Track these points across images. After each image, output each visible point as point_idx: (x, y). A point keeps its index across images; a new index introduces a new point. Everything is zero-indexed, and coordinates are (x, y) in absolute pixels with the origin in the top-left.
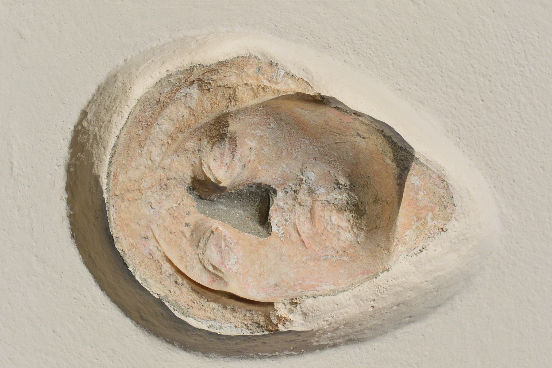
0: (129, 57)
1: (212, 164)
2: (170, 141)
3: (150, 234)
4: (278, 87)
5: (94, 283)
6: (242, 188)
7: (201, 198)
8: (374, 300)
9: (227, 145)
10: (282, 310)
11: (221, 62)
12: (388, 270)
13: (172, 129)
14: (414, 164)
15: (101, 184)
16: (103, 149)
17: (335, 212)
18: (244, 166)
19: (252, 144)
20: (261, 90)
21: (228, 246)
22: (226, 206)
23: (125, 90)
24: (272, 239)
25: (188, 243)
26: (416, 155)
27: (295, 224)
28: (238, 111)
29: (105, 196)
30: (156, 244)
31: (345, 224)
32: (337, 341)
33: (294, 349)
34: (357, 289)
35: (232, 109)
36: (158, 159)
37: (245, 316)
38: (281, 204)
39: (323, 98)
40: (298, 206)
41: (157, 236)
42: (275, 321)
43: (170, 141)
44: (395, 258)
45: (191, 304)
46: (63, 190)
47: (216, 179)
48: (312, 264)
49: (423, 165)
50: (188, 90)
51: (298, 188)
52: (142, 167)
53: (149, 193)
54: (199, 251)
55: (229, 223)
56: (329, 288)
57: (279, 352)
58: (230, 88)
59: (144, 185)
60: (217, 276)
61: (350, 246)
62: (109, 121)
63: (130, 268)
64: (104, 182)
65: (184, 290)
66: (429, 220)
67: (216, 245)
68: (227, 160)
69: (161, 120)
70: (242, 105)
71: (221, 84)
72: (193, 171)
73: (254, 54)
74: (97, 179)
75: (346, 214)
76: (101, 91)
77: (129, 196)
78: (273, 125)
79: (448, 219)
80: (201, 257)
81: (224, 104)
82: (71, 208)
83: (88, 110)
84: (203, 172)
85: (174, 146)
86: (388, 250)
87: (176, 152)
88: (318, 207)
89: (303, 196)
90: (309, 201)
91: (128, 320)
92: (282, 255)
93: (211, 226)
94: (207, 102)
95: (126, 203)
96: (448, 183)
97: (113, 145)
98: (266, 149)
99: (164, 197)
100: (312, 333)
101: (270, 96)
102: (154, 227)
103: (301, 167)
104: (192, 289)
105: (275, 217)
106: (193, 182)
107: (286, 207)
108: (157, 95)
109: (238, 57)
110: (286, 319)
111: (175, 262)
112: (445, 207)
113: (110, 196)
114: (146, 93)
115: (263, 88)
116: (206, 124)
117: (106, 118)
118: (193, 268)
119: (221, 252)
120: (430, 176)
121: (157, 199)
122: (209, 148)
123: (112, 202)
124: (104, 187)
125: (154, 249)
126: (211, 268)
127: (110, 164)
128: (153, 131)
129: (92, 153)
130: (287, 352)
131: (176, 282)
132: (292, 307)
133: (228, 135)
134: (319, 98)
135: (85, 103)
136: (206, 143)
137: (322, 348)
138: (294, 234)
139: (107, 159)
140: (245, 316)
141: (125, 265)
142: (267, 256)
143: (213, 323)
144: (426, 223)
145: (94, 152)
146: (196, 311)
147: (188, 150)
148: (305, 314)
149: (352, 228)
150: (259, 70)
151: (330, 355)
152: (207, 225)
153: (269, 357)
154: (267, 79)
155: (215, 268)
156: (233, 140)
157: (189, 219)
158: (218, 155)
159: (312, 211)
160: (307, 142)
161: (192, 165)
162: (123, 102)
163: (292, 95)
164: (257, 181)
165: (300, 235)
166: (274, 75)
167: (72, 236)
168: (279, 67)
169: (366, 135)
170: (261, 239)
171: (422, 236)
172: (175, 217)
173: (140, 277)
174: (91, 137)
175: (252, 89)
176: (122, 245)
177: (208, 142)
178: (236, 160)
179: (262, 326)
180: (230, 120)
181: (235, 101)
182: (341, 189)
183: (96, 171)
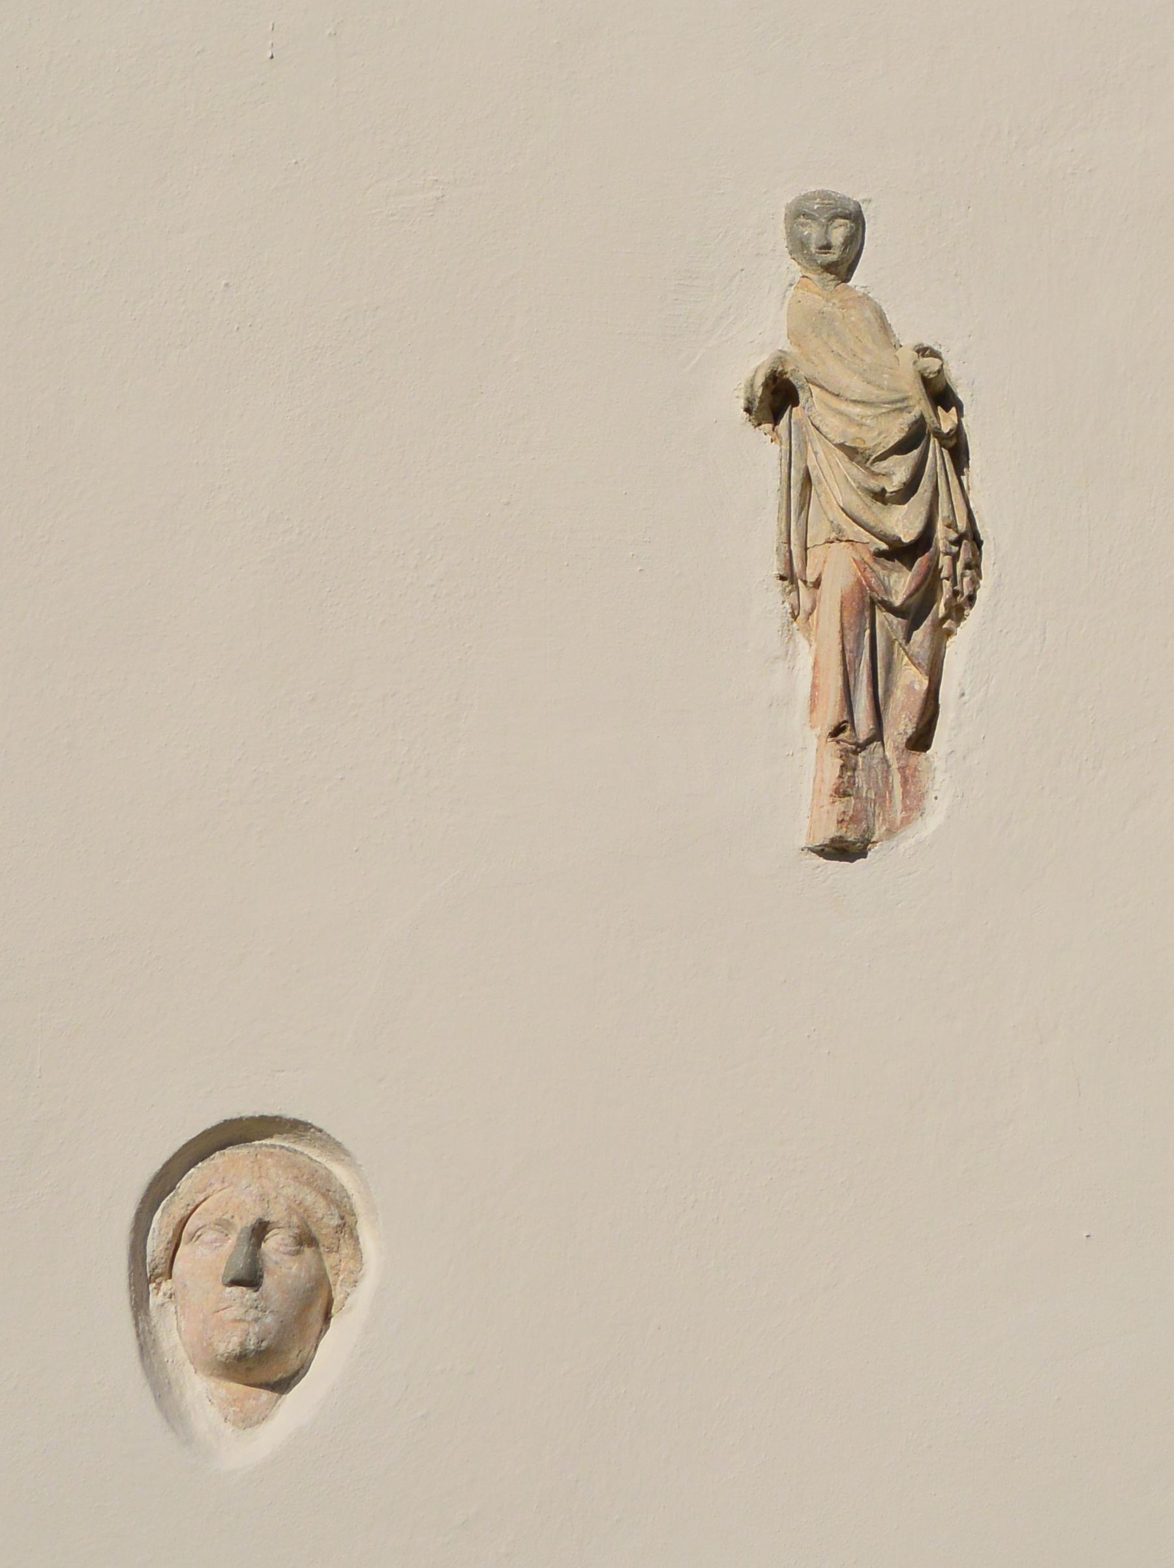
0: (363, 1169)
1: (279, 1237)
3: (226, 1184)
4: (338, 1286)
5: (189, 1139)
6: (260, 1262)
7: (253, 1230)
8: (173, 1361)
9: (293, 1248)
10: (166, 1286)
11: (358, 1239)
12: (196, 1372)
13: (307, 1204)
14: (277, 1395)
15: (266, 1140)
16: (293, 1141)
17: (240, 1340)
18: (277, 1263)
19: (294, 1270)
20: (336, 1272)
23: (339, 1161)
24: (220, 1287)
25: (218, 1217)
26: (283, 1396)
27: (231, 1307)
28: (320, 1254)
29: (257, 1142)
30: (219, 1189)
31: (231, 1347)
32: (142, 1337)
33: (136, 1302)
34: (182, 1348)
35: (322, 1249)
36: (284, 1192)
37: (162, 1258)
38: (247, 1296)
39: (330, 1319)
40: (246, 1309)
41: (224, 1191)
42: (158, 1281)
43: (297, 1202)
44: (205, 1379)
46: (261, 1114)
47: (267, 1239)
49: (276, 1401)
50: (337, 1216)
51: (259, 1309)
52: (278, 1180)
53: (257, 1185)
54: (212, 1225)
56: (183, 1325)
57: (134, 1290)
58: (338, 1248)
59: (264, 1181)
60: (193, 1237)
62: (315, 1147)
63: (200, 1164)
64: (267, 1142)
65: (182, 1212)
66: (233, 1409)
67: (216, 1239)
68: (282, 1249)
69: (314, 1193)
70: (324, 1257)
71: (341, 1242)
72: (273, 1222)
73: (364, 1268)
74: (270, 1136)
75: (239, 1348)
76: (338, 1145)
77: (256, 1168)
78: (308, 1285)
80: (208, 1227)
81: (326, 1244)
82: (247, 1119)
83: (323, 1133)
84: (273, 1229)
85: (294, 1206)
86: (211, 1375)
87: (289, 1208)
88: (243, 1326)
89: (253, 1313)
90: (249, 1318)
91: (160, 1167)
92: (208, 1293)
95: (250, 1165)
96: (261, 1423)
98: (290, 1282)
99: (254, 1198)
100: (147, 1314)
101: (331, 1279)
102: (231, 1188)
104: (184, 1217)
105: (237, 1291)
106: (265, 1222)
107: (245, 1300)
108: (333, 1189)
109: (362, 1254)
110: (159, 1289)
112: (243, 1421)
113: (256, 1148)
114: (336, 1178)
115: (337, 1273)
116: (310, 1231)
117: (317, 1144)
118: (200, 1219)
119: (212, 1243)
120: (267, 1409)
121: (254, 1192)
122: (291, 1234)
123: (252, 1150)
124: (264, 1142)
125: (214, 1188)
126: (199, 1233)
127: (282, 1147)
128: (306, 1187)
129: (290, 1133)
130: (133, 1296)
131: (188, 1205)
133: (302, 1248)
134: (329, 1316)
135: (328, 1132)
137: (137, 1325)
138: (225, 1305)
139: (286, 1144)
140: (162, 1258)
141: (202, 1160)
143: (157, 1233)
144: (231, 1407)
145: (291, 1135)
146: (166, 1220)
147: (290, 1217)
148: (163, 1305)
150: (352, 1272)
151: (132, 1332)
152: (232, 1232)
153: (130, 1282)
154: (344, 1278)
155: (199, 1236)
156: (298, 1252)
157: (237, 1218)
158: (286, 1242)
160: (295, 1314)
161: (278, 1221)
162: (329, 1158)
163: (331, 1295)
164: (265, 1275)
165: (223, 1310)
166: (347, 1284)
167: (226, 1121)
168: (354, 1288)
169: (299, 1357)
170: (221, 1277)
172: (238, 1207)
173: (193, 1173)
174: (303, 1133)
175: (337, 1265)
176: (218, 1158)
177: (296, 1233)
178: (281, 1255)
179: (154, 1271)
180: (313, 1248)
181: (328, 1252)
182: (258, 1343)
183: (276, 1136)
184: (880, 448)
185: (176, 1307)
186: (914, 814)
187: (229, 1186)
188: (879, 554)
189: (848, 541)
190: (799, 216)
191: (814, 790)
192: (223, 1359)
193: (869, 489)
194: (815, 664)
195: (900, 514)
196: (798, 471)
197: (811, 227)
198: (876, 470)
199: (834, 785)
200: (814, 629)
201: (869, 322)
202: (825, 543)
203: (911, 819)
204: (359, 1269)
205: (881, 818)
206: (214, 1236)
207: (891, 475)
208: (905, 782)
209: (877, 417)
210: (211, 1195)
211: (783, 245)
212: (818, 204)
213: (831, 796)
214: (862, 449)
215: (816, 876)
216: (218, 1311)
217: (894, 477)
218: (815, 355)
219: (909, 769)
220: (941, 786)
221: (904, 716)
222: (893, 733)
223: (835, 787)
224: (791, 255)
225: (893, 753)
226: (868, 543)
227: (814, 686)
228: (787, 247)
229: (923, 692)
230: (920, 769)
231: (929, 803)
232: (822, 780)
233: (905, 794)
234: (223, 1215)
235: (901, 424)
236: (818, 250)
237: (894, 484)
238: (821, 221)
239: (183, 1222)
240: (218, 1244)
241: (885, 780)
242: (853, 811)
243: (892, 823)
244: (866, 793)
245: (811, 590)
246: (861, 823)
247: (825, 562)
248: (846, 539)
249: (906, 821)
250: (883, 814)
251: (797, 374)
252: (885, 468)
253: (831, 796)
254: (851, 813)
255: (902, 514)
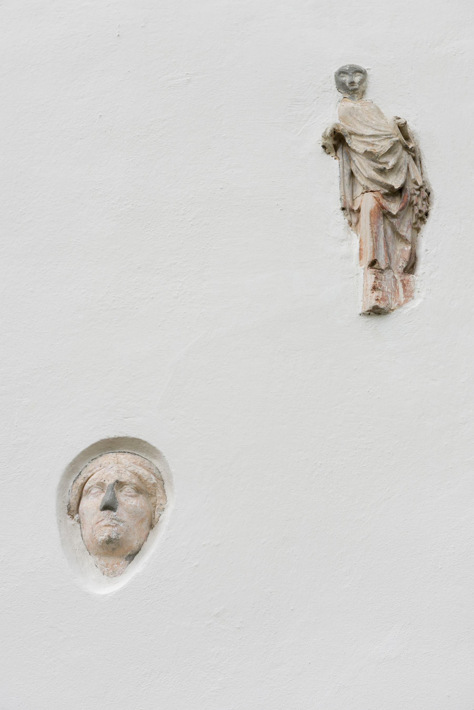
2: (135, 473)
6: (117, 499)
12: (90, 554)
20: (155, 505)
21: (97, 496)
22: (110, 494)
24: (99, 512)
25: (98, 481)
27: (104, 519)
30: (98, 470)
41: (101, 470)
43: (135, 473)
44: (94, 557)
45: (77, 483)
48: (91, 527)
49: (128, 565)
53: (116, 467)
54: (96, 486)
55: (105, 496)
60: (87, 492)
61: (96, 540)
62: (144, 452)
67: (98, 492)
73: (167, 503)
79: (108, 575)
80: (93, 486)
88: (110, 528)
93: (104, 489)
94: (150, 486)
97: (135, 453)
103: (125, 521)
105: (106, 512)
109: (166, 497)
111: (92, 477)
119: (95, 493)
126: (90, 490)
131: (85, 478)
132: (77, 520)
136: (135, 486)
138: (100, 519)
142: (93, 510)
149: (103, 540)
154: (158, 507)
159: (109, 525)
160: (135, 523)
162: (151, 456)
165: (100, 521)
168: (163, 512)
171: (102, 566)
184: (382, 152)
185: (80, 526)
186: (409, 299)
187: (103, 468)
188: (386, 194)
189: (371, 191)
190: (340, 74)
191: (363, 290)
192: (101, 544)
193: (379, 168)
194: (360, 241)
195: (393, 179)
196: (347, 170)
197: (346, 77)
198: (381, 161)
199: (372, 285)
200: (359, 230)
201: (373, 110)
202: (361, 194)
203: (408, 301)
204: (165, 503)
205: (394, 300)
206: (97, 490)
207: (388, 162)
208: (404, 286)
209: (380, 141)
210: (95, 473)
211: (334, 87)
212: (348, 68)
213: (371, 290)
214: (374, 152)
215: (367, 325)
216: (98, 523)
217: (389, 163)
218: (351, 124)
219: (406, 281)
220: (420, 287)
221: (401, 260)
222: (397, 267)
223: (373, 286)
224: (338, 90)
225: (397, 274)
226: (380, 191)
227: (360, 249)
228: (336, 88)
229: (409, 250)
230: (410, 280)
231: (415, 294)
232: (367, 285)
233: (405, 291)
234: (100, 480)
235: (390, 141)
236: (350, 85)
237: (389, 166)
238: (350, 74)
239: (83, 485)
240: (98, 494)
241: (395, 285)
242: (382, 296)
243: (400, 302)
244: (387, 289)
245: (356, 214)
246: (386, 301)
247: (361, 201)
248: (370, 191)
249: (406, 301)
250: (395, 298)
251: (345, 128)
252: (385, 160)
253: (371, 290)
254: (381, 297)
255: (394, 179)
